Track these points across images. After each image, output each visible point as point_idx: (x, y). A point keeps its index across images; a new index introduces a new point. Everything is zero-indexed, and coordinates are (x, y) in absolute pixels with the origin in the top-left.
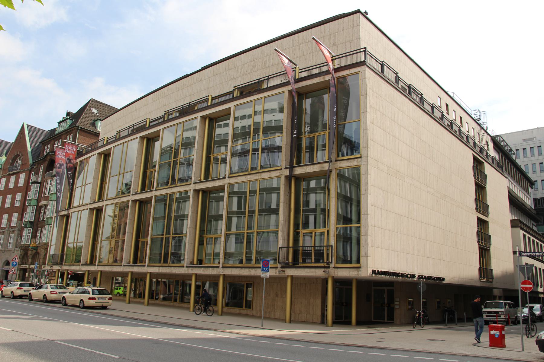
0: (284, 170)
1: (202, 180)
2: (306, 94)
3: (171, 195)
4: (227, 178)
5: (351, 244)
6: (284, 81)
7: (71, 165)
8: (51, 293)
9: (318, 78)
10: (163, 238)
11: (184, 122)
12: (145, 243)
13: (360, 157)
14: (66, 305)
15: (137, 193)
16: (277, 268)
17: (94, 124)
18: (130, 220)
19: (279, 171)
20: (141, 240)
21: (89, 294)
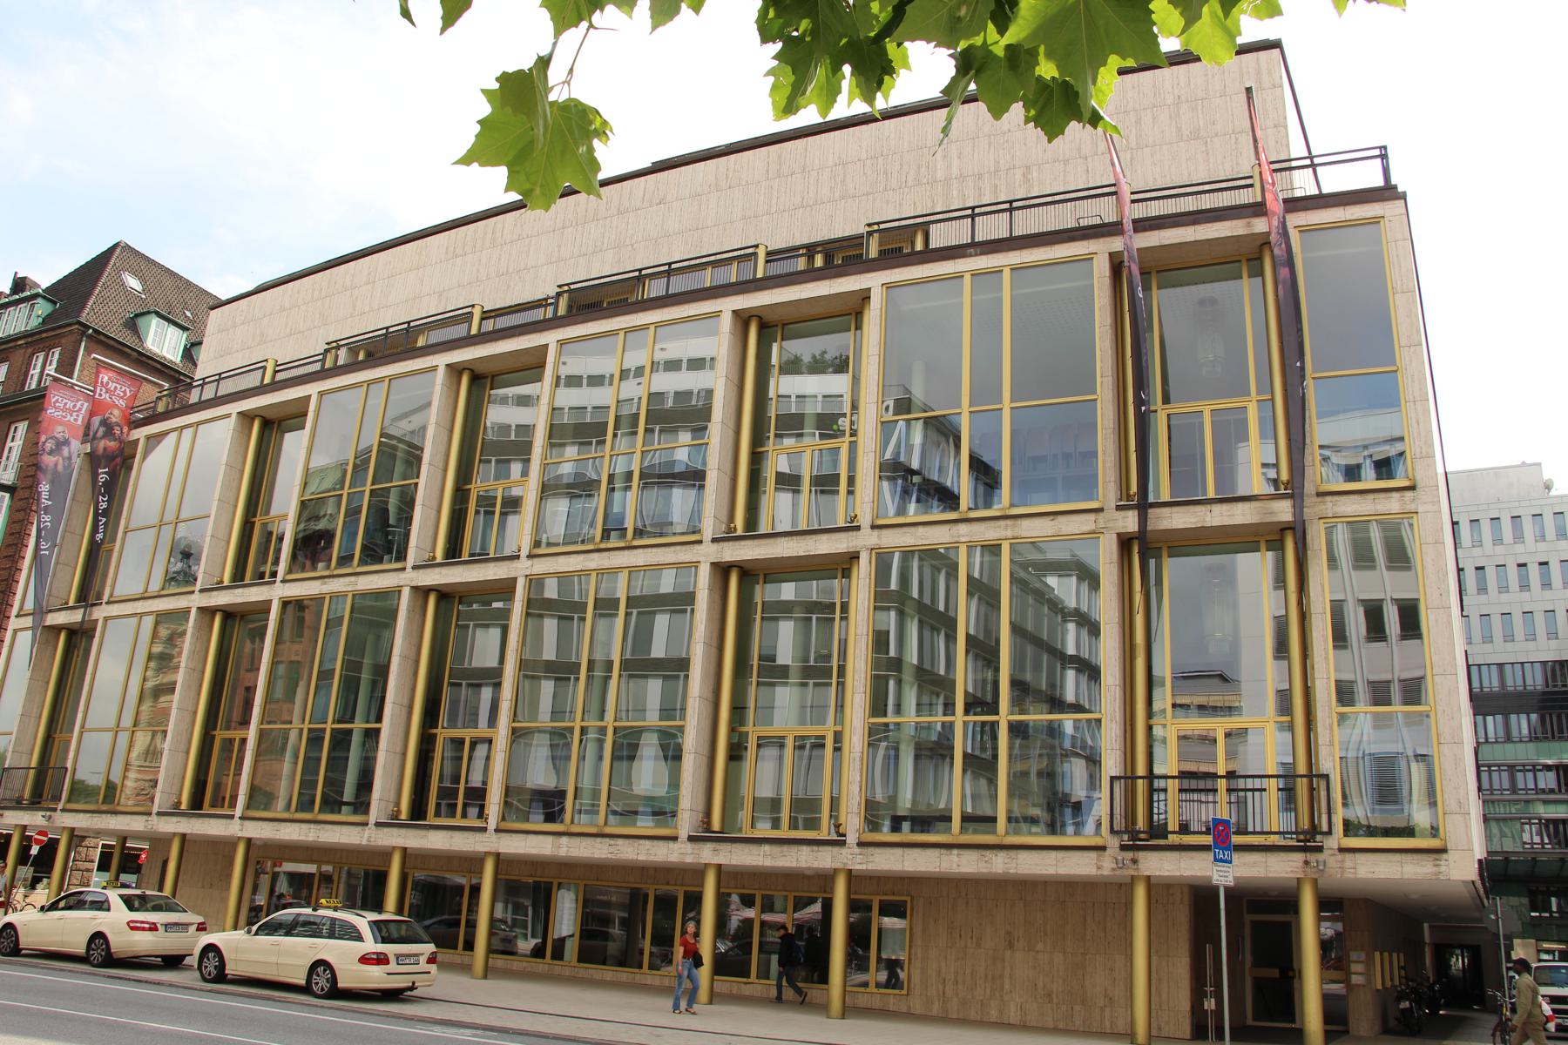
1: (439, 560)
2: (280, 422)
4: (866, 529)
6: (1084, 223)
7: (112, 444)
8: (133, 927)
9: (1227, 224)
11: (392, 378)
13: (1412, 488)
14: (221, 977)
15: (430, 564)
16: (1103, 848)
17: (132, 325)
18: (404, 657)
19: (1092, 517)
20: (220, 734)
21: (360, 938)
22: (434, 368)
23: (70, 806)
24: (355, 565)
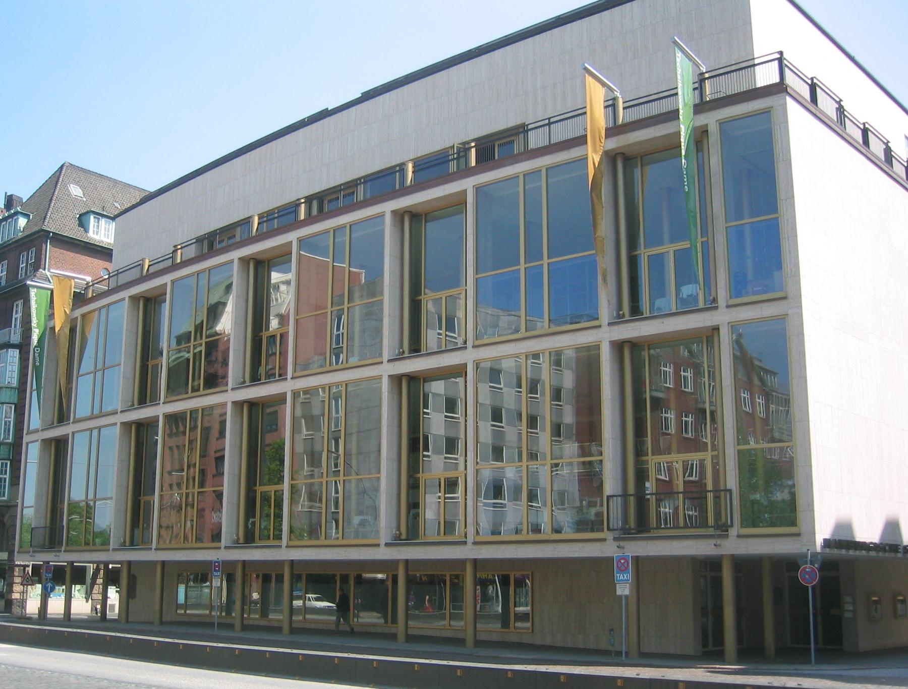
0: (605, 328)
3: (194, 412)
5: (776, 482)
10: (322, 483)
12: (149, 506)
13: (785, 298)
19: (594, 331)
22: (232, 261)
23: (69, 548)
24: (202, 392)
